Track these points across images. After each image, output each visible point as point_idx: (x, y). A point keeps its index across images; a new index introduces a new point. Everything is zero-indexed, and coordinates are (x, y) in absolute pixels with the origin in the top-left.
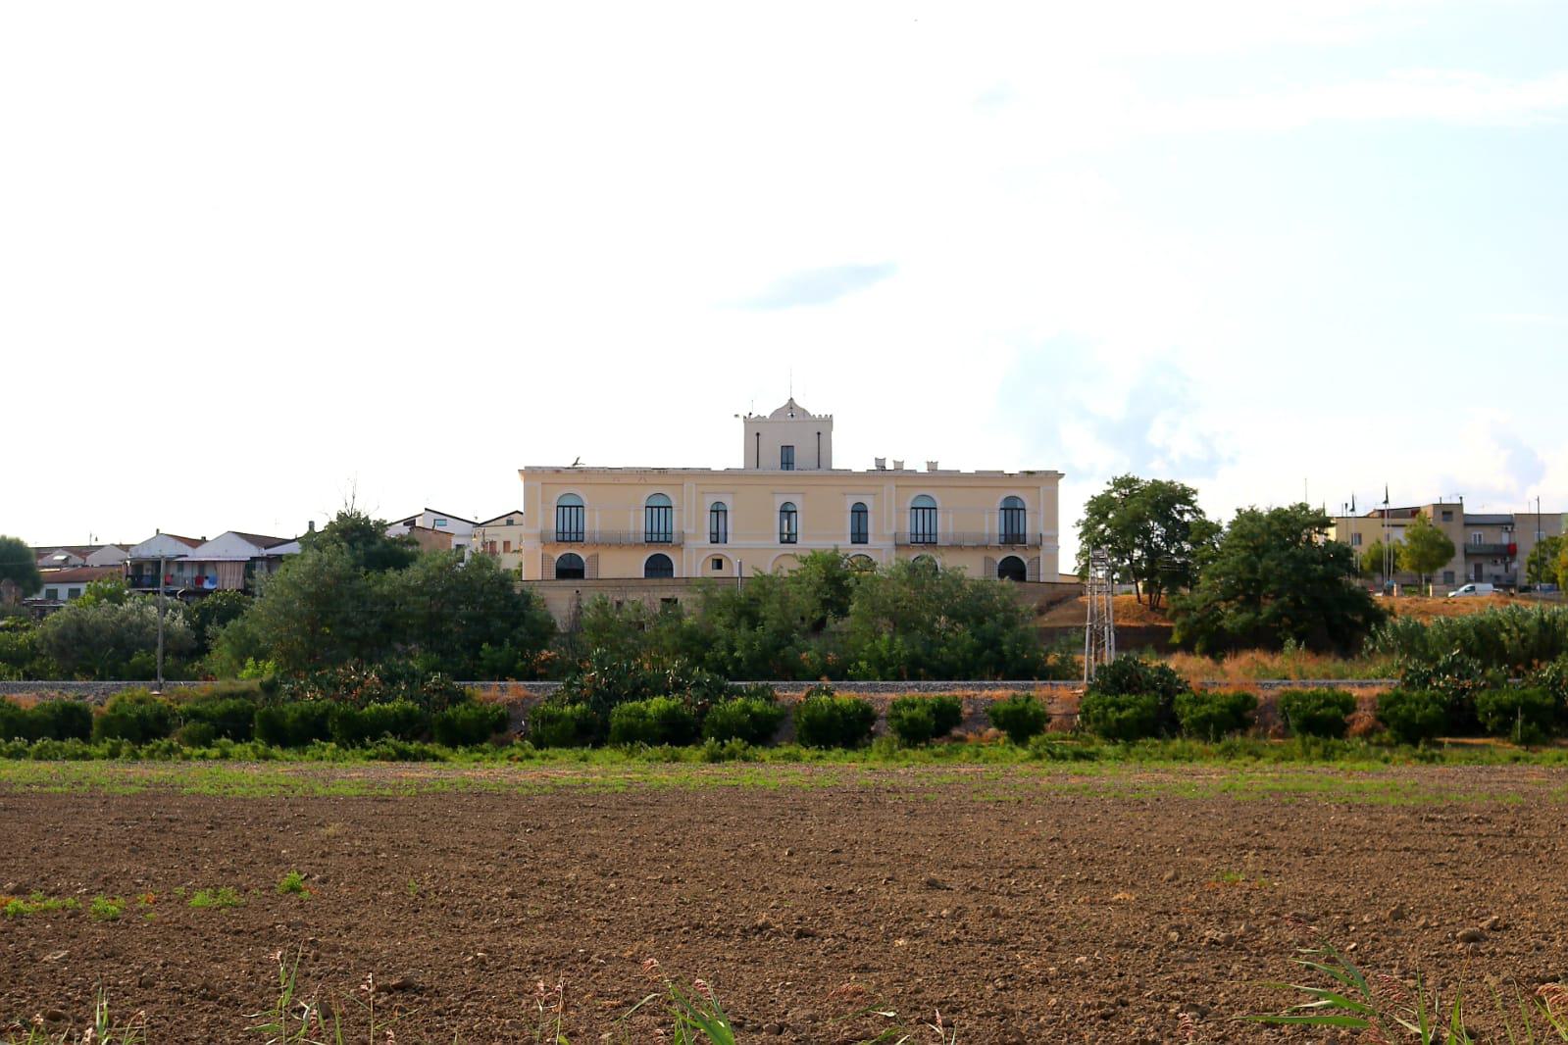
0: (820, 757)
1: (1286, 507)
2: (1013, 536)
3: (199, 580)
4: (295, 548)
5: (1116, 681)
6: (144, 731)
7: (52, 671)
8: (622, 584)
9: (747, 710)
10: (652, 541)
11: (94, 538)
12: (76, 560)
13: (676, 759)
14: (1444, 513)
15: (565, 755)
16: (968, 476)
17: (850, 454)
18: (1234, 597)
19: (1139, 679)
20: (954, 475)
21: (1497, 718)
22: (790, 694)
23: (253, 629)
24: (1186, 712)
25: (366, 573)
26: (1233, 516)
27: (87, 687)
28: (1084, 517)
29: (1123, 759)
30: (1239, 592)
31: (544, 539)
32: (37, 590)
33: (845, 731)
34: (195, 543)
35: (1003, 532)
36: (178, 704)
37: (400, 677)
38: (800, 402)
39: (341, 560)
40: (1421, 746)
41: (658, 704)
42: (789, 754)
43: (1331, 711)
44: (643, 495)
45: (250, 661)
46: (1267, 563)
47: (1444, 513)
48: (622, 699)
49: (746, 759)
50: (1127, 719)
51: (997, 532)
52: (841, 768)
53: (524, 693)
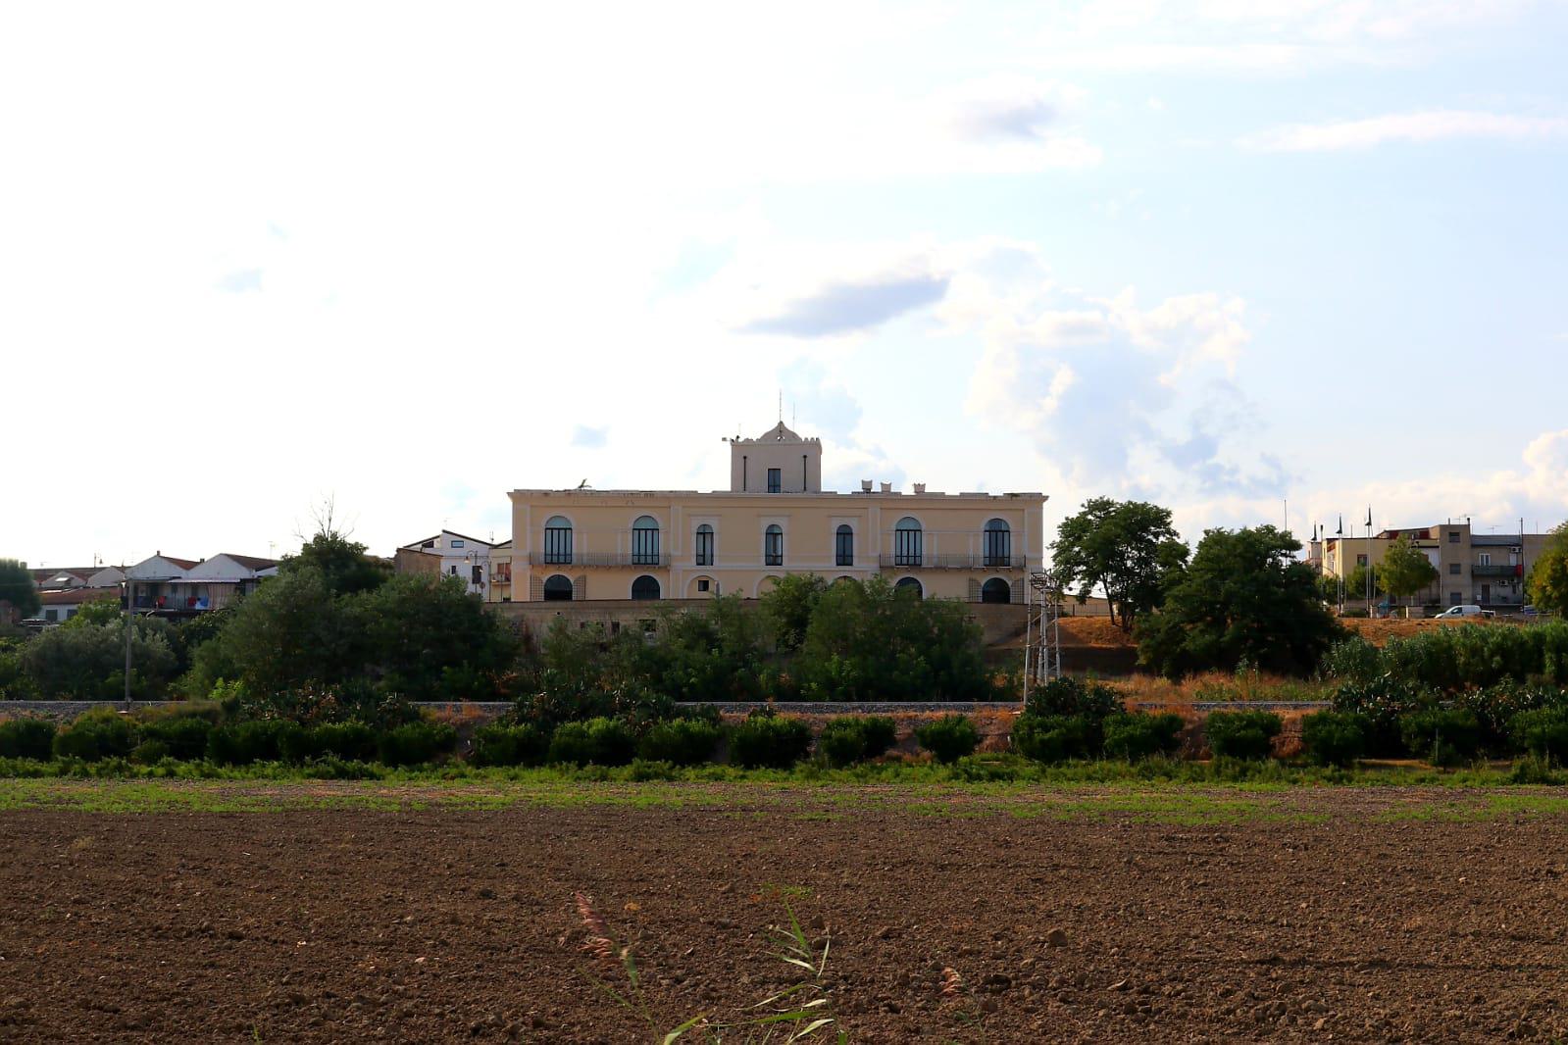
0: (743, 777)
1: (1253, 529)
2: (997, 557)
3: (192, 602)
4: (273, 571)
5: (1051, 702)
6: (104, 749)
7: (34, 690)
8: (616, 604)
9: (683, 730)
10: (639, 563)
11: (98, 560)
12: (78, 581)
13: (604, 778)
14: (1451, 534)
15: (496, 774)
16: (952, 499)
17: (838, 475)
18: (1201, 619)
19: (1074, 699)
20: (940, 498)
21: (1418, 739)
22: (735, 714)
23: (225, 650)
24: (1111, 732)
25: (338, 596)
26: (1202, 537)
27: (58, 707)
28: (1058, 539)
29: (1038, 780)
30: (1206, 614)
31: (532, 561)
32: (36, 611)
33: (778, 751)
34: (188, 565)
35: (987, 554)
36: (143, 723)
37: (356, 697)
38: (788, 425)
39: (315, 581)
40: (1331, 767)
41: (598, 724)
42: (713, 774)
43: (1251, 733)
44: (630, 519)
45: (220, 682)
46: (1230, 584)
47: (1451, 534)
48: (564, 717)
49: (670, 779)
50: (1050, 740)
51: (981, 554)
52: (765, 786)
53: (480, 713)
